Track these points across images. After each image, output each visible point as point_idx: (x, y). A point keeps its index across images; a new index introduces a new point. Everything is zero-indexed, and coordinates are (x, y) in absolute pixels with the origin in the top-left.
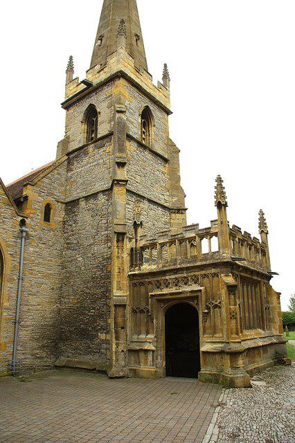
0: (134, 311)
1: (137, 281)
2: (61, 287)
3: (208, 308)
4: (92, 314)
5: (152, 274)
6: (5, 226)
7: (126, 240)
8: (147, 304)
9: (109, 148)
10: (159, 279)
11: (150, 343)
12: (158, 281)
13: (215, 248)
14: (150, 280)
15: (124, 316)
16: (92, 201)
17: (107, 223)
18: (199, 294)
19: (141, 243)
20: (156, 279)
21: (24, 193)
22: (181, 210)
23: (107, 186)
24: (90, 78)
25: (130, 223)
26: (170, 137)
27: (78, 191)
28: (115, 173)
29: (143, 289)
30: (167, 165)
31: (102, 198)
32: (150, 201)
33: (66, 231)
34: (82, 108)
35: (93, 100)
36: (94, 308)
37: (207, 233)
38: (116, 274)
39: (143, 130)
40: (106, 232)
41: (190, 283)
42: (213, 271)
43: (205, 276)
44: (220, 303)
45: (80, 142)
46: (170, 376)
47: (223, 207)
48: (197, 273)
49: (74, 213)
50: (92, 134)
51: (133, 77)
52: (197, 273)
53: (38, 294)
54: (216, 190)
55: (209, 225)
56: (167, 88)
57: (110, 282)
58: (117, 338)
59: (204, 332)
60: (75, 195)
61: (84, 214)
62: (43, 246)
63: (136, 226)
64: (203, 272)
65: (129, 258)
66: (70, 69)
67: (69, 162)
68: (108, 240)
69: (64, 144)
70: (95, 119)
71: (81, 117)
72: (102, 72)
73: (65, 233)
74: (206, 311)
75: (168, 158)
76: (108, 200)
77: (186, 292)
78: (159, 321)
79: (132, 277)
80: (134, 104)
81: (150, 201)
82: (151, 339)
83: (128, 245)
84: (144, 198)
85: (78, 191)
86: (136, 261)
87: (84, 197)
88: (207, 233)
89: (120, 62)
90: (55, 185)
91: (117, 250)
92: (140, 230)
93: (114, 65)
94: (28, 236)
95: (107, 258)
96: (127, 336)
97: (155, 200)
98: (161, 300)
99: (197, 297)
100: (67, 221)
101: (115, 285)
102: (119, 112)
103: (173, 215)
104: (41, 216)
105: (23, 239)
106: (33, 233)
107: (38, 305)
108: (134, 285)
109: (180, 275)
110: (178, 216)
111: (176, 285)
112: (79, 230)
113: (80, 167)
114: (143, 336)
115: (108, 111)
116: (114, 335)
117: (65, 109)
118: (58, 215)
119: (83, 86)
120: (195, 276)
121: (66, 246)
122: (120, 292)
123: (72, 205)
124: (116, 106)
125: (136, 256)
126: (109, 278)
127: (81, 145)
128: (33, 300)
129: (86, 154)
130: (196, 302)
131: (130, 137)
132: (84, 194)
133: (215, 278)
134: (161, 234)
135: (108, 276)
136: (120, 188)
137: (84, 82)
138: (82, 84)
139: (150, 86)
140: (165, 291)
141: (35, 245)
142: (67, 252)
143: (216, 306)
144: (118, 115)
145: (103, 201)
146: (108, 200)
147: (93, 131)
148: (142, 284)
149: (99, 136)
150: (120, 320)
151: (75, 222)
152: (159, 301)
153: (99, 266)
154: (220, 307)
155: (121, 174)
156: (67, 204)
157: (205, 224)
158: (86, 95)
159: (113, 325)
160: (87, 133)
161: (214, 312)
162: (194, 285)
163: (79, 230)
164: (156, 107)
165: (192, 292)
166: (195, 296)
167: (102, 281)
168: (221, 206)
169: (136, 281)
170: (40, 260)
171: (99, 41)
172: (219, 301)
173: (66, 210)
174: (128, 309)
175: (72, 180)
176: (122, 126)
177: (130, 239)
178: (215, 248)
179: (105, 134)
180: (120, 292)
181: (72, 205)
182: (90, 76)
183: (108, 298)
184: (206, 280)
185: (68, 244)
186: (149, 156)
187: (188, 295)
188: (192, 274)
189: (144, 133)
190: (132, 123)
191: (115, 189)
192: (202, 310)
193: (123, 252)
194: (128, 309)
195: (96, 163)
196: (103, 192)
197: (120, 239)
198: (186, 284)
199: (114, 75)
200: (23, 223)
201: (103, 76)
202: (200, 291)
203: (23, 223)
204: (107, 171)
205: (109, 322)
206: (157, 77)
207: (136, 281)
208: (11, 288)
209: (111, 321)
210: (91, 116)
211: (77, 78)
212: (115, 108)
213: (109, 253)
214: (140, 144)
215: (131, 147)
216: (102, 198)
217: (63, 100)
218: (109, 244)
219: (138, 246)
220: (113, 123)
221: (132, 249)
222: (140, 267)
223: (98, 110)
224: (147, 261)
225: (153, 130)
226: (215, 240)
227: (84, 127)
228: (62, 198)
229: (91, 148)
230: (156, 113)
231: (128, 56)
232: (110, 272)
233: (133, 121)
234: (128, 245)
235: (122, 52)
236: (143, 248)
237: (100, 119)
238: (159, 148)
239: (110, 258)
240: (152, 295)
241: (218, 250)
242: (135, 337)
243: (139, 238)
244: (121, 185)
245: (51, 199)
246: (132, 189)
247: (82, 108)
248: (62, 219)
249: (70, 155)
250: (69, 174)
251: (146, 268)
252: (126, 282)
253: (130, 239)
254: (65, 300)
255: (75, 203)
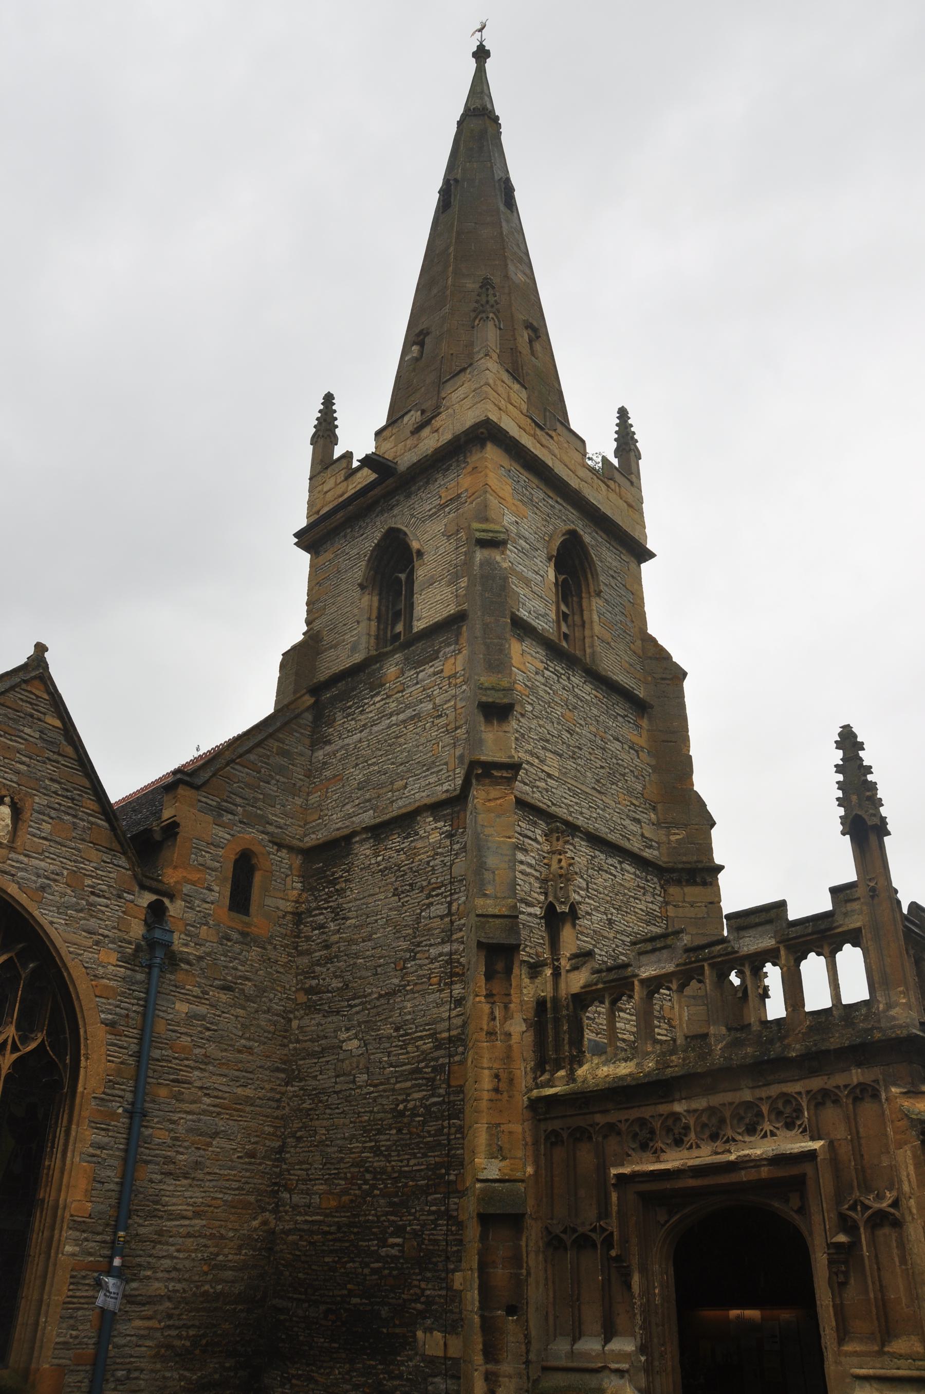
0: (554, 1243)
1: (567, 1123)
2: (281, 1150)
3: (846, 1224)
4: (394, 1252)
5: (620, 1093)
6: (93, 923)
7: (520, 974)
8: (604, 1213)
9: (454, 661)
10: (647, 1112)
11: (620, 1373)
12: (642, 1122)
13: (855, 990)
14: (612, 1117)
15: (516, 1260)
16: (395, 841)
17: (450, 914)
18: (808, 1168)
19: (577, 981)
20: (634, 1114)
21: (167, 814)
22: (706, 873)
23: (445, 785)
24: (390, 451)
25: (531, 914)
26: (651, 631)
27: (349, 809)
28: (474, 741)
29: (586, 1156)
30: (645, 723)
31: (432, 831)
32: (596, 841)
33: (304, 946)
34: (369, 537)
35: (399, 518)
36: (400, 1231)
37: (822, 935)
38: (486, 1096)
39: (563, 608)
40: (446, 949)
41: (767, 1127)
42: (856, 1076)
43: (822, 1098)
44: (895, 1204)
45: (354, 649)
46: (248, 910)
47: (873, 838)
48: (792, 1088)
49: (334, 883)
50: (393, 626)
51: (526, 441)
52: (792, 1088)
53: (199, 1174)
54: (840, 777)
55: (826, 905)
56: (634, 480)
57: (460, 1130)
58: (491, 1353)
59: (843, 1335)
60: (335, 822)
61: (369, 890)
62: (224, 997)
63: (555, 919)
64: (816, 1083)
65: (529, 1038)
66: (326, 430)
67: (321, 716)
68: (453, 972)
69: (296, 662)
70: (403, 576)
71: (358, 572)
72: (426, 432)
73: (301, 954)
74: (842, 1238)
75: (651, 694)
76: (450, 836)
77: (756, 1163)
78: (651, 1282)
79: (541, 1108)
80: (527, 525)
81: (596, 841)
82: (622, 1356)
83: (528, 990)
84: (572, 829)
85: (349, 809)
86: (558, 1048)
87: (366, 829)
88: (822, 935)
89: (483, 396)
90: (271, 789)
91: (486, 1008)
92: (567, 933)
93: (462, 411)
94: (173, 960)
95: (450, 1039)
96: (528, 1344)
97: (612, 837)
98: (656, 1192)
99: (798, 1184)
100: (309, 911)
101: (481, 1138)
102: (484, 544)
103: (672, 890)
104: (221, 893)
105: (156, 971)
106: (190, 950)
107: (197, 1215)
108: (554, 1139)
109: (728, 1097)
110: (692, 892)
111: (714, 1137)
112: (351, 942)
113: (357, 733)
114: (591, 1345)
115: (445, 546)
116: (478, 1340)
117: (306, 548)
118: (281, 889)
119: (367, 476)
120: (787, 1098)
121: (302, 998)
122: (495, 1158)
123: (326, 858)
124: (476, 525)
125: (557, 1031)
126: (458, 1113)
127: (358, 658)
128: (179, 1197)
129: (376, 686)
130: (795, 1202)
131: (522, 628)
132: (368, 818)
133: (868, 1108)
134: (649, 946)
135: (453, 1109)
136: (495, 792)
137: (367, 461)
138: (366, 471)
139: (582, 473)
140: (672, 1160)
141: (197, 991)
142: (306, 1021)
143: (880, 1219)
144: (480, 555)
145: (435, 837)
146: (450, 836)
147: (397, 616)
148: (581, 1135)
149: (419, 625)
150: (500, 1274)
151: (338, 914)
152: (647, 1199)
153: (418, 1070)
154: (897, 1224)
155: (495, 744)
156: (310, 854)
157: (808, 902)
158: (376, 503)
159: (473, 1297)
160: (379, 618)
161: (873, 1242)
162: (782, 1133)
163: (351, 942)
164: (600, 538)
165: (779, 1160)
166: (791, 1174)
167: (432, 1127)
168: (864, 822)
169: (556, 1125)
170: (211, 1048)
171: (415, 348)
172: (890, 1196)
173: (304, 877)
174: (532, 1237)
175: (328, 773)
176: (494, 588)
177: (535, 969)
178: (855, 990)
179: (438, 618)
180: (495, 1158)
181: (326, 858)
182: (387, 446)
183: (454, 1190)
184: (831, 1115)
185: (310, 991)
186: (586, 691)
187: (765, 1172)
188: (774, 1090)
189: (565, 616)
190: (527, 582)
191: (479, 795)
192: (822, 1238)
193: (507, 1016)
194: (532, 1237)
195: (409, 713)
196: (435, 808)
197: (500, 966)
198: (751, 1130)
199: (466, 433)
200: (157, 912)
201: (430, 442)
202: (811, 1155)
203: (157, 912)
204: (447, 740)
205: (457, 1285)
206: (601, 445)
207: (556, 1125)
208: (101, 1147)
209: (466, 1281)
210: (393, 567)
211: (348, 456)
212: (474, 515)
213: (458, 1021)
214: (554, 650)
215: (524, 659)
216: (432, 831)
217: (302, 523)
218: (457, 990)
219: (563, 992)
220: (464, 582)
221: (541, 1004)
222: (572, 1072)
223: (415, 545)
224: (599, 1050)
225: (596, 609)
226: (851, 960)
227: (368, 602)
228: (294, 832)
229: (391, 669)
230: (604, 555)
231: (505, 376)
232: (461, 1090)
233: (531, 575)
234: (528, 990)
235: (491, 369)
236: (582, 1000)
237: (421, 573)
238: (616, 664)
239: (458, 1041)
240: (619, 1176)
241: (867, 997)
242: (561, 1346)
243: (565, 964)
244: (496, 781)
245: (252, 836)
246: (536, 798)
247: (369, 537)
248: (289, 907)
249: (314, 686)
250: (320, 754)
251: (597, 1071)
252: (518, 1128)
253: (535, 969)
254: (296, 1199)
255: (337, 848)
